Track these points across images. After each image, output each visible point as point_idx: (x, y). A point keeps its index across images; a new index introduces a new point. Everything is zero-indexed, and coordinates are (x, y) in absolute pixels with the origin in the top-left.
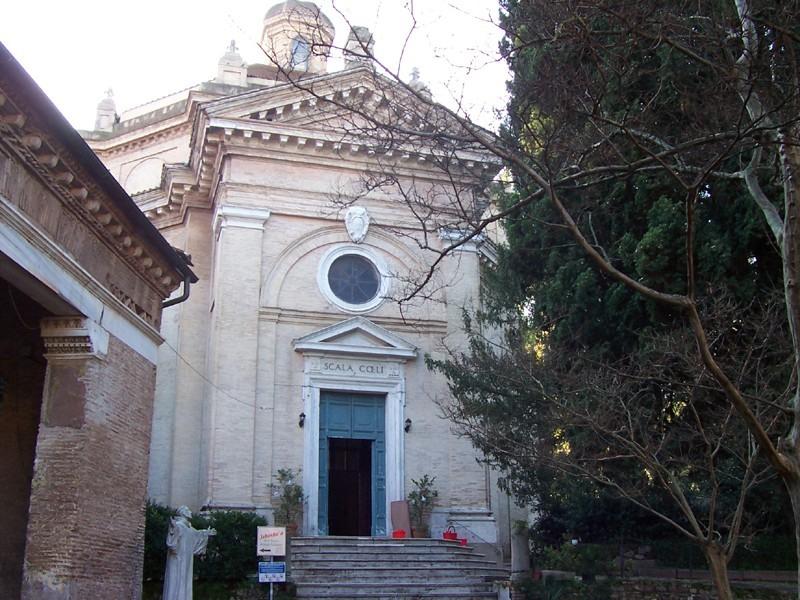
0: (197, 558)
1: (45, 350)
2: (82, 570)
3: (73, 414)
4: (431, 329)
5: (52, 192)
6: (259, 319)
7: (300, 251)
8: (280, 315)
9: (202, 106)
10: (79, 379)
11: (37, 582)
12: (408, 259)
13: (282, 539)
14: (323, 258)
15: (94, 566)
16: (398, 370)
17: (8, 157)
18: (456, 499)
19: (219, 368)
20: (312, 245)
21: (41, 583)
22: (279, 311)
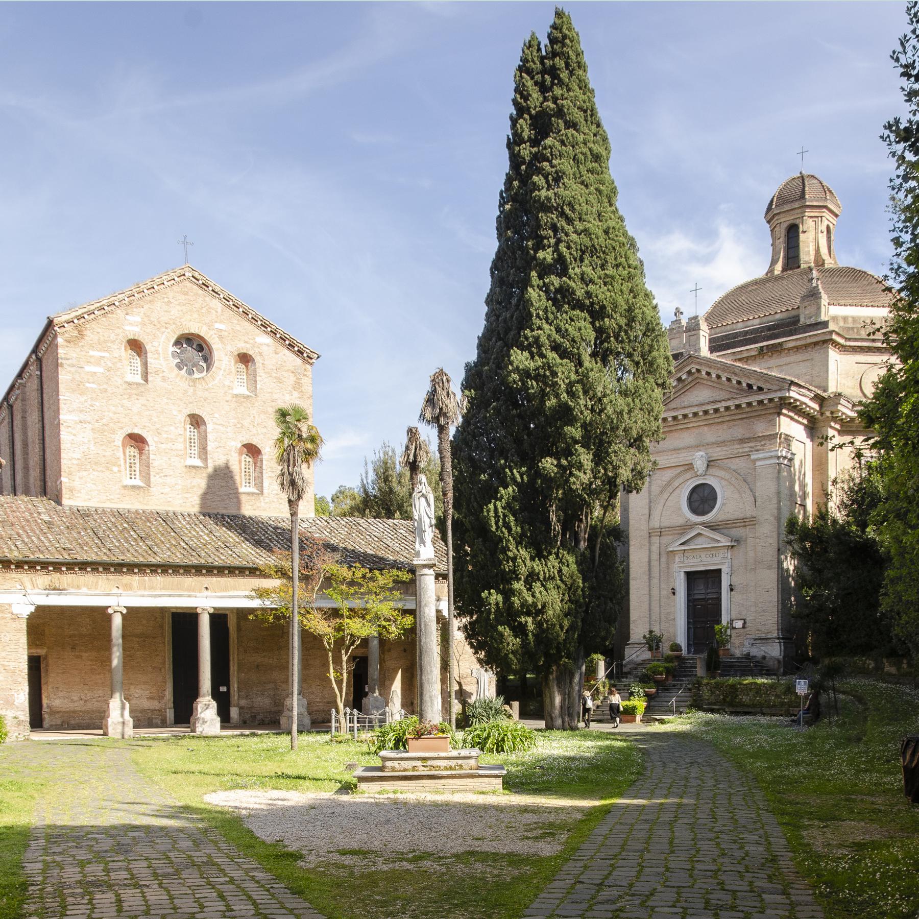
2: (162, 867)
7: (670, 489)
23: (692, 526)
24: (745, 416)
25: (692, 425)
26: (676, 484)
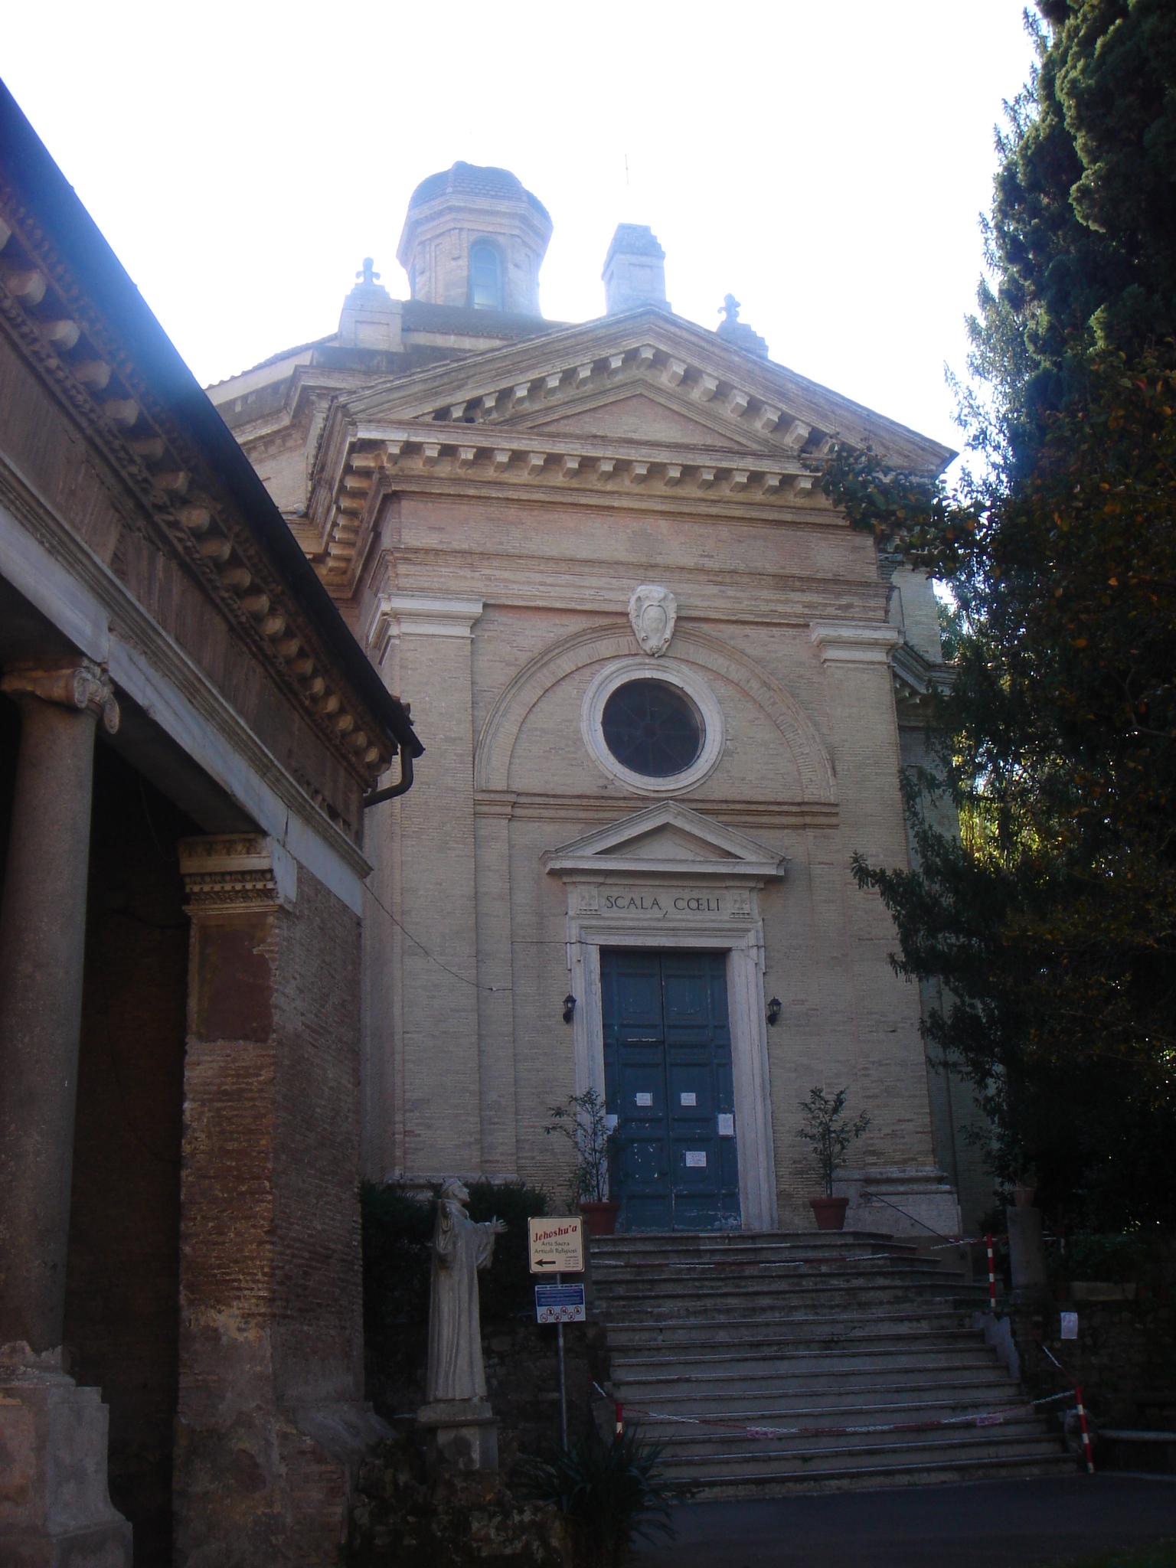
0: (482, 1273)
1: (187, 899)
3: (246, 1014)
4: (808, 820)
5: (216, 606)
6: (476, 815)
7: (545, 678)
8: (514, 805)
9: (342, 399)
10: (255, 951)
11: (207, 1327)
12: (755, 684)
13: (575, 1240)
14: (591, 689)
15: (298, 1296)
16: (751, 903)
17: (159, 549)
18: (873, 1153)
19: (403, 913)
20: (565, 664)
21: (216, 1330)
22: (512, 798)
23: (640, 803)
24: (789, 517)
25: (625, 503)
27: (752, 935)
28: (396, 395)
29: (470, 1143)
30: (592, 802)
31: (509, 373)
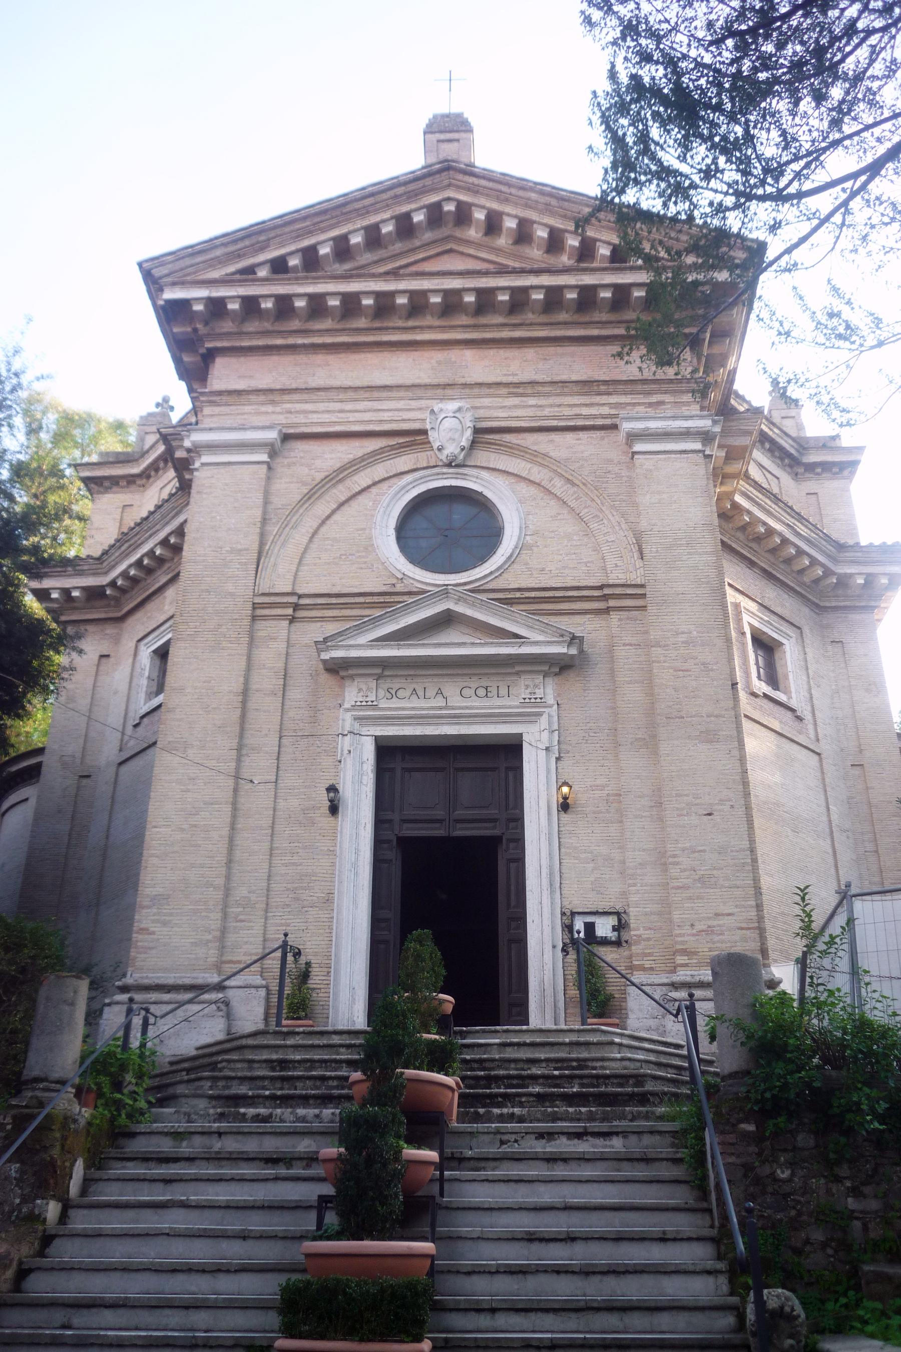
6: (254, 618)
7: (341, 492)
18: (684, 952)
22: (294, 599)
23: (421, 595)
26: (362, 479)
27: (544, 720)
28: (200, 259)
29: (208, 941)
30: (376, 599)
31: (310, 233)
